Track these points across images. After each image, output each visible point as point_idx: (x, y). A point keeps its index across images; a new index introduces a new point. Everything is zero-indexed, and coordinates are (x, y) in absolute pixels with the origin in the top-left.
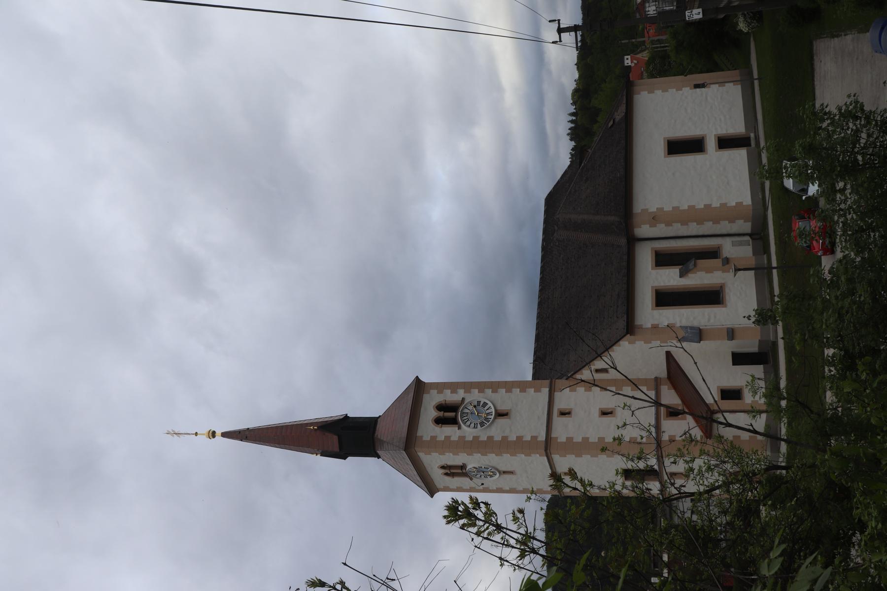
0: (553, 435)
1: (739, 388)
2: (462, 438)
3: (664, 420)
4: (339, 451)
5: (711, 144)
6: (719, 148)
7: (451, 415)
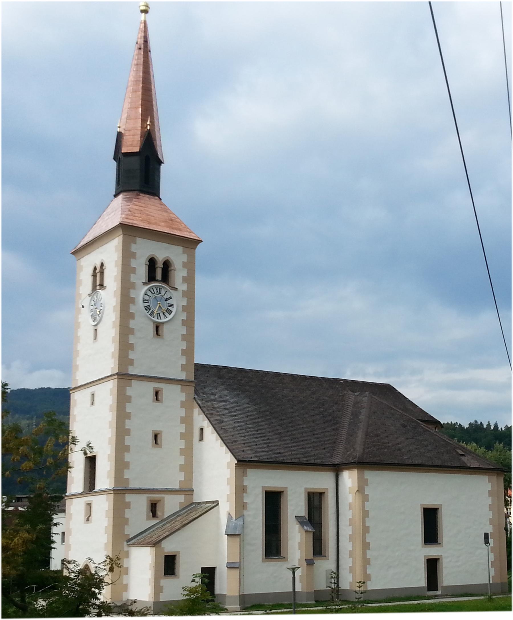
0: (134, 382)
1: (176, 571)
2: (133, 286)
3: (147, 497)
4: (123, 152)
5: (432, 551)
6: (427, 560)
7: (159, 275)
